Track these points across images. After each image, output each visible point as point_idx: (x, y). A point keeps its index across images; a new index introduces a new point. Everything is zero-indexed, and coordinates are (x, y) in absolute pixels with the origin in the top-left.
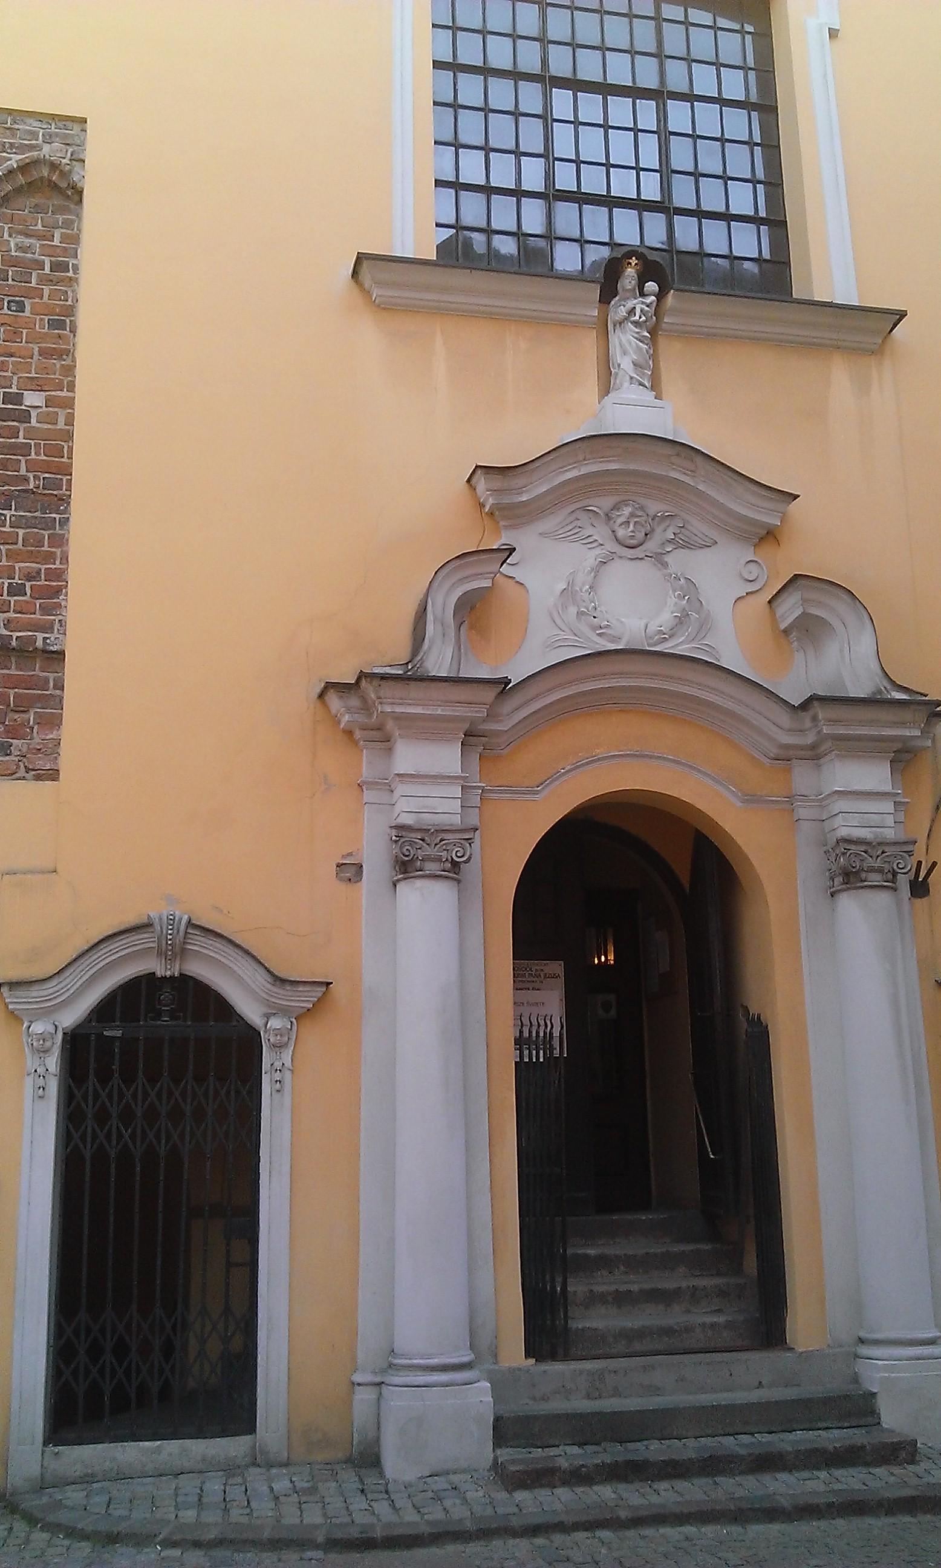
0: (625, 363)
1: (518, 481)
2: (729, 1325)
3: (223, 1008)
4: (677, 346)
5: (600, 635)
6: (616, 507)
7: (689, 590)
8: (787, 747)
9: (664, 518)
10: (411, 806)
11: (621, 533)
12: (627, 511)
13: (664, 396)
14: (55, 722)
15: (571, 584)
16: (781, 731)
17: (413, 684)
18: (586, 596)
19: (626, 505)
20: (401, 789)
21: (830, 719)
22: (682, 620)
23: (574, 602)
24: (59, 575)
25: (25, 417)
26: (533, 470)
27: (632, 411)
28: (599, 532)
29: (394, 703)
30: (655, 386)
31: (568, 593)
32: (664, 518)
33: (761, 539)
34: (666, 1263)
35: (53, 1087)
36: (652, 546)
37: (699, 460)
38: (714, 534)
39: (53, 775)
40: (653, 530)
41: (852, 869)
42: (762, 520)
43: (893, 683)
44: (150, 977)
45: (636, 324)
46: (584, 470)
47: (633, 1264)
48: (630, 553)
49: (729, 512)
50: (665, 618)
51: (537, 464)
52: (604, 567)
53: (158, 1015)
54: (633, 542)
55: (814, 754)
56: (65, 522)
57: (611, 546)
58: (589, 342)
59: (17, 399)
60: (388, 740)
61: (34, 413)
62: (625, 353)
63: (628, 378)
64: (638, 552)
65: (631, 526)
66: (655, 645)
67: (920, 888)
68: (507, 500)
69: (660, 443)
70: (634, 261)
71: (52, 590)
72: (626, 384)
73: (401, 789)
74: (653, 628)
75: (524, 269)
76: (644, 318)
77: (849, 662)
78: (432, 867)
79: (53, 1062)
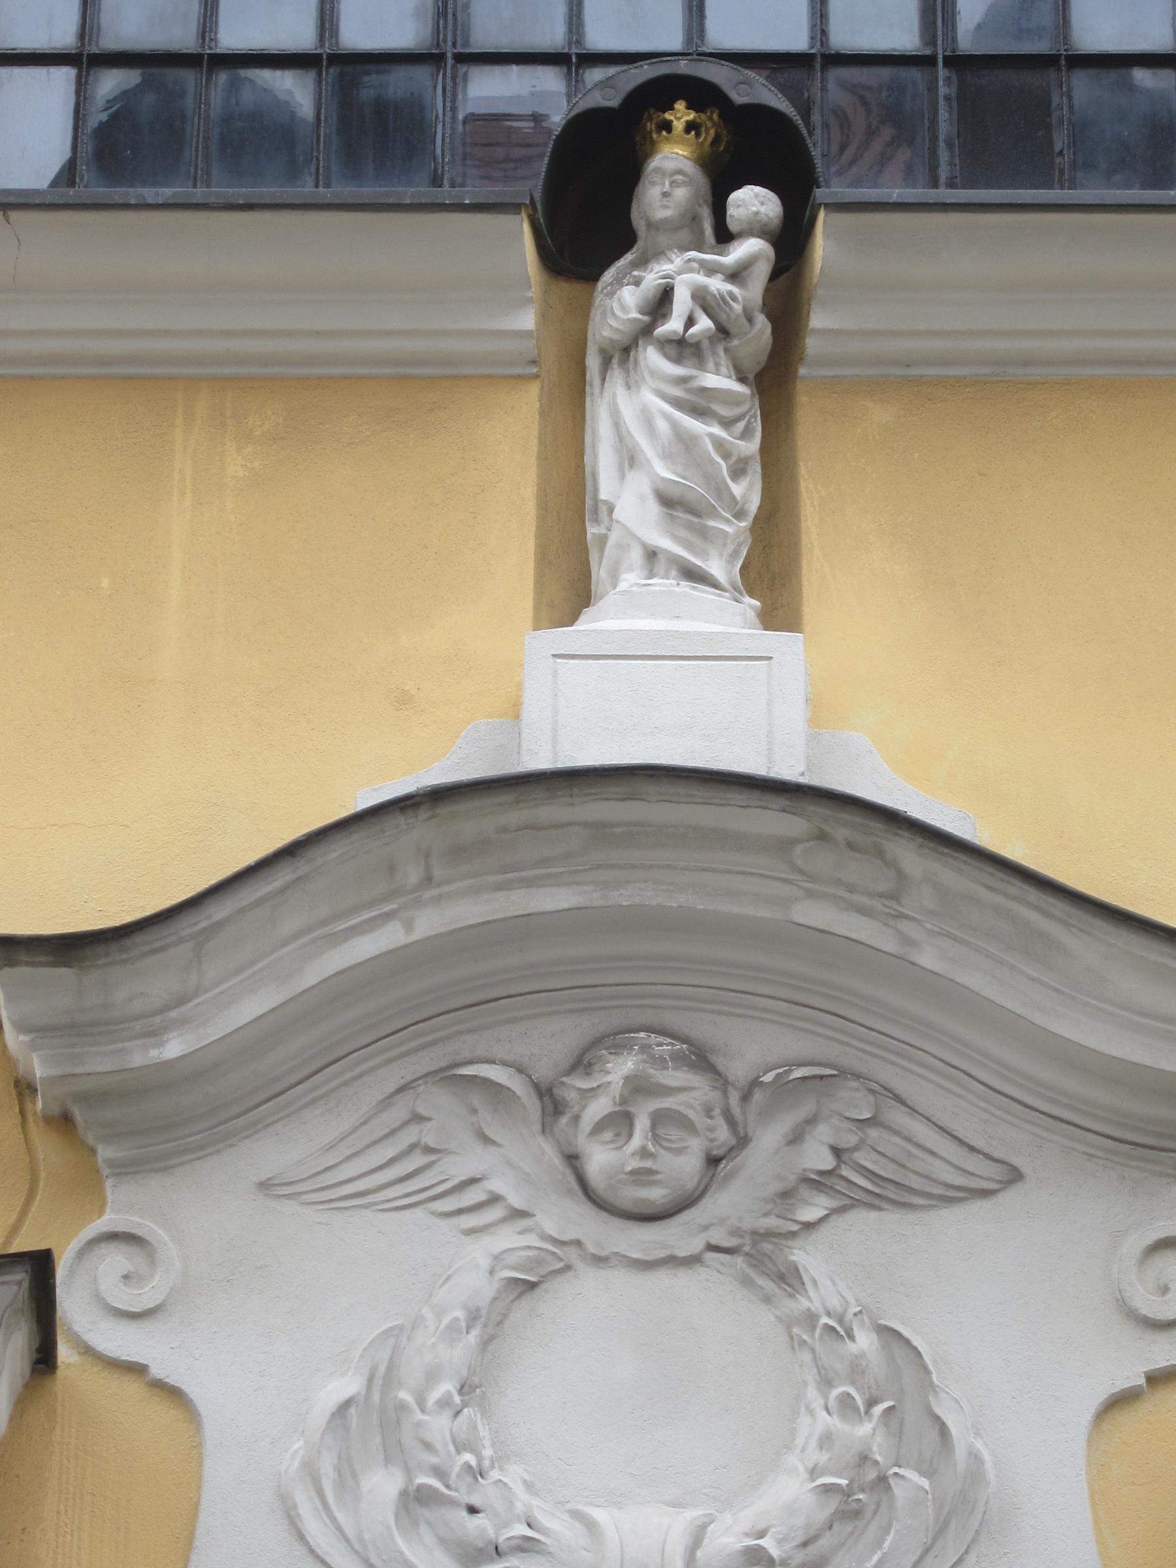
0: (629, 504)
1: (140, 983)
4: (880, 414)
6: (582, 1063)
7: (898, 1387)
9: (786, 1091)
11: (601, 1159)
12: (621, 1068)
13: (811, 609)
15: (384, 1378)
18: (439, 1426)
19: (618, 1049)
23: (394, 1453)
27: (665, 674)
28: (511, 1164)
30: (772, 579)
31: (373, 1420)
32: (786, 1091)
36: (733, 1205)
37: (909, 856)
38: (1012, 1140)
40: (743, 1141)
45: (682, 348)
46: (430, 922)
52: (526, 1303)
54: (656, 1195)
58: (510, 434)
62: (630, 459)
63: (636, 555)
65: (642, 1124)
68: (100, 1062)
69: (739, 797)
70: (681, 115)
72: (631, 578)
75: (102, 192)
76: (704, 323)
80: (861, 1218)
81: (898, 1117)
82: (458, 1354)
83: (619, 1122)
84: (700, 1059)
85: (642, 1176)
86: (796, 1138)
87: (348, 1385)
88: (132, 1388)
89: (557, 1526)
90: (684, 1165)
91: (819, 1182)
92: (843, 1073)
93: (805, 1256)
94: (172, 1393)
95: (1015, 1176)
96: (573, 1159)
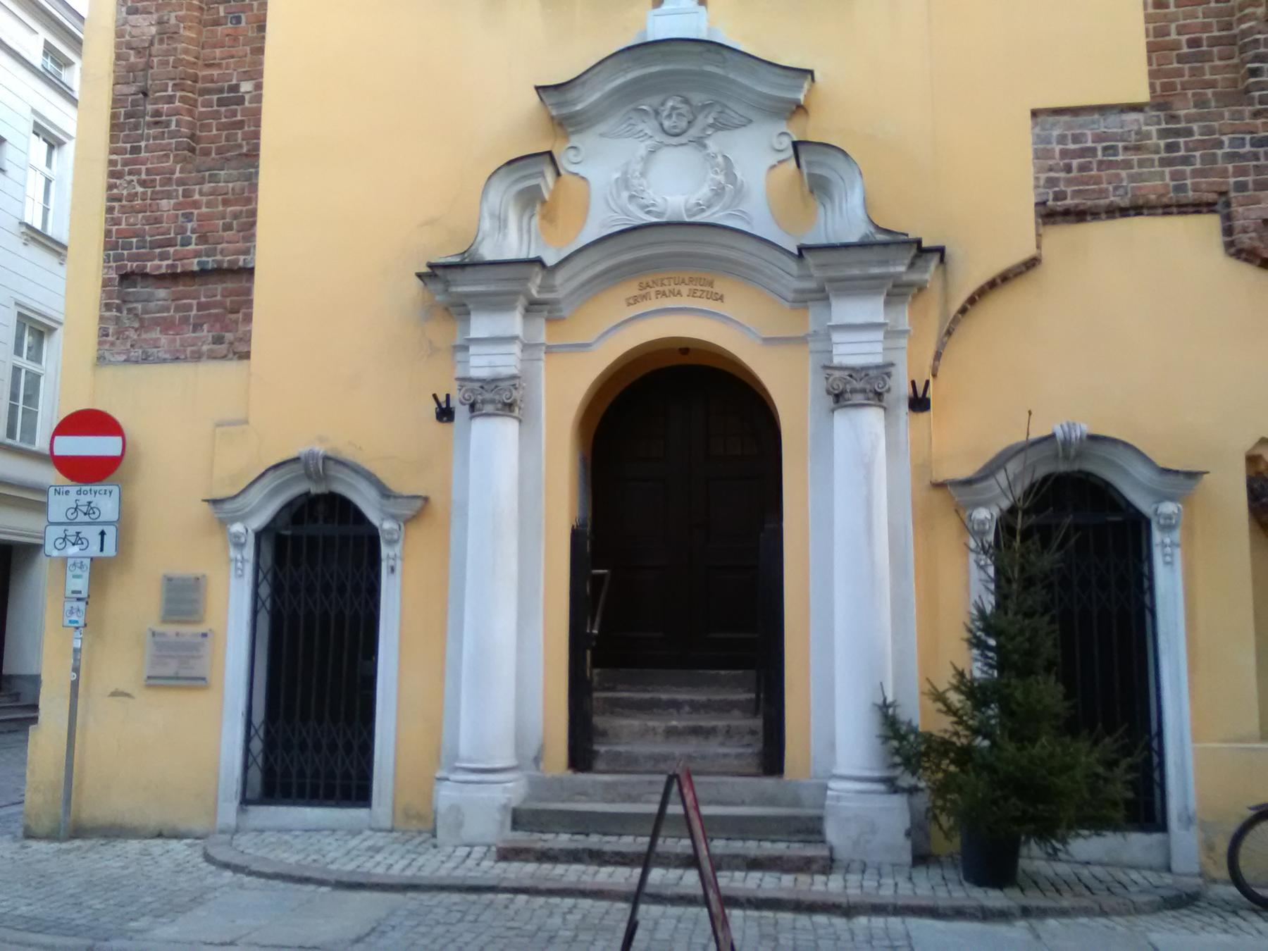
1: (573, 94)
2: (738, 756)
3: (360, 517)
5: (648, 212)
6: (663, 104)
8: (802, 291)
9: (704, 107)
10: (481, 364)
11: (667, 124)
14: (248, 318)
15: (625, 173)
16: (790, 278)
17: (469, 270)
18: (635, 182)
20: (836, 337)
21: (825, 270)
22: (718, 192)
23: (627, 187)
24: (253, 213)
25: (241, 101)
26: (584, 83)
28: (649, 126)
29: (465, 286)
31: (624, 182)
32: (704, 107)
33: (793, 113)
34: (724, 708)
35: (249, 570)
36: (694, 132)
38: (750, 114)
39: (246, 356)
40: (695, 117)
41: (851, 389)
42: (784, 93)
43: (877, 227)
44: (307, 494)
47: (696, 707)
48: (675, 140)
49: (760, 94)
50: (705, 192)
51: (586, 77)
53: (316, 521)
54: (677, 131)
55: (821, 295)
56: (257, 173)
57: (660, 137)
59: (235, 88)
60: (827, 298)
61: (247, 97)
64: (682, 139)
66: (694, 215)
67: (919, 403)
68: (565, 111)
71: (248, 226)
73: (473, 349)
74: (693, 201)
77: (846, 220)
78: (489, 408)
79: (249, 552)
80: (720, 133)
81: (727, 111)
82: (639, 167)
83: (669, 116)
84: (686, 101)
85: (675, 127)
86: (706, 117)
87: (617, 175)
88: (576, 178)
89: (659, 200)
90: (684, 124)
91: (711, 126)
92: (717, 102)
93: (709, 142)
94: (583, 178)
95: (750, 121)
96: (661, 125)
